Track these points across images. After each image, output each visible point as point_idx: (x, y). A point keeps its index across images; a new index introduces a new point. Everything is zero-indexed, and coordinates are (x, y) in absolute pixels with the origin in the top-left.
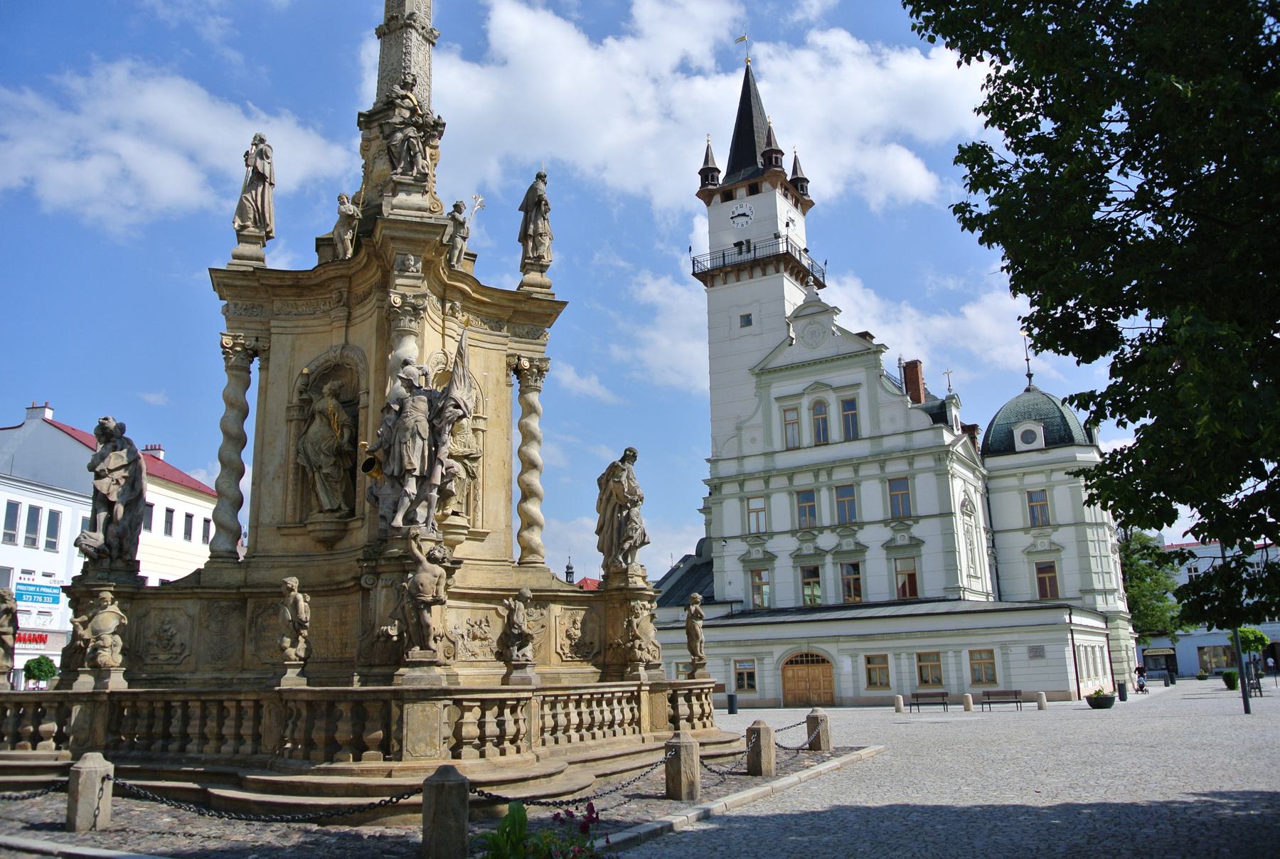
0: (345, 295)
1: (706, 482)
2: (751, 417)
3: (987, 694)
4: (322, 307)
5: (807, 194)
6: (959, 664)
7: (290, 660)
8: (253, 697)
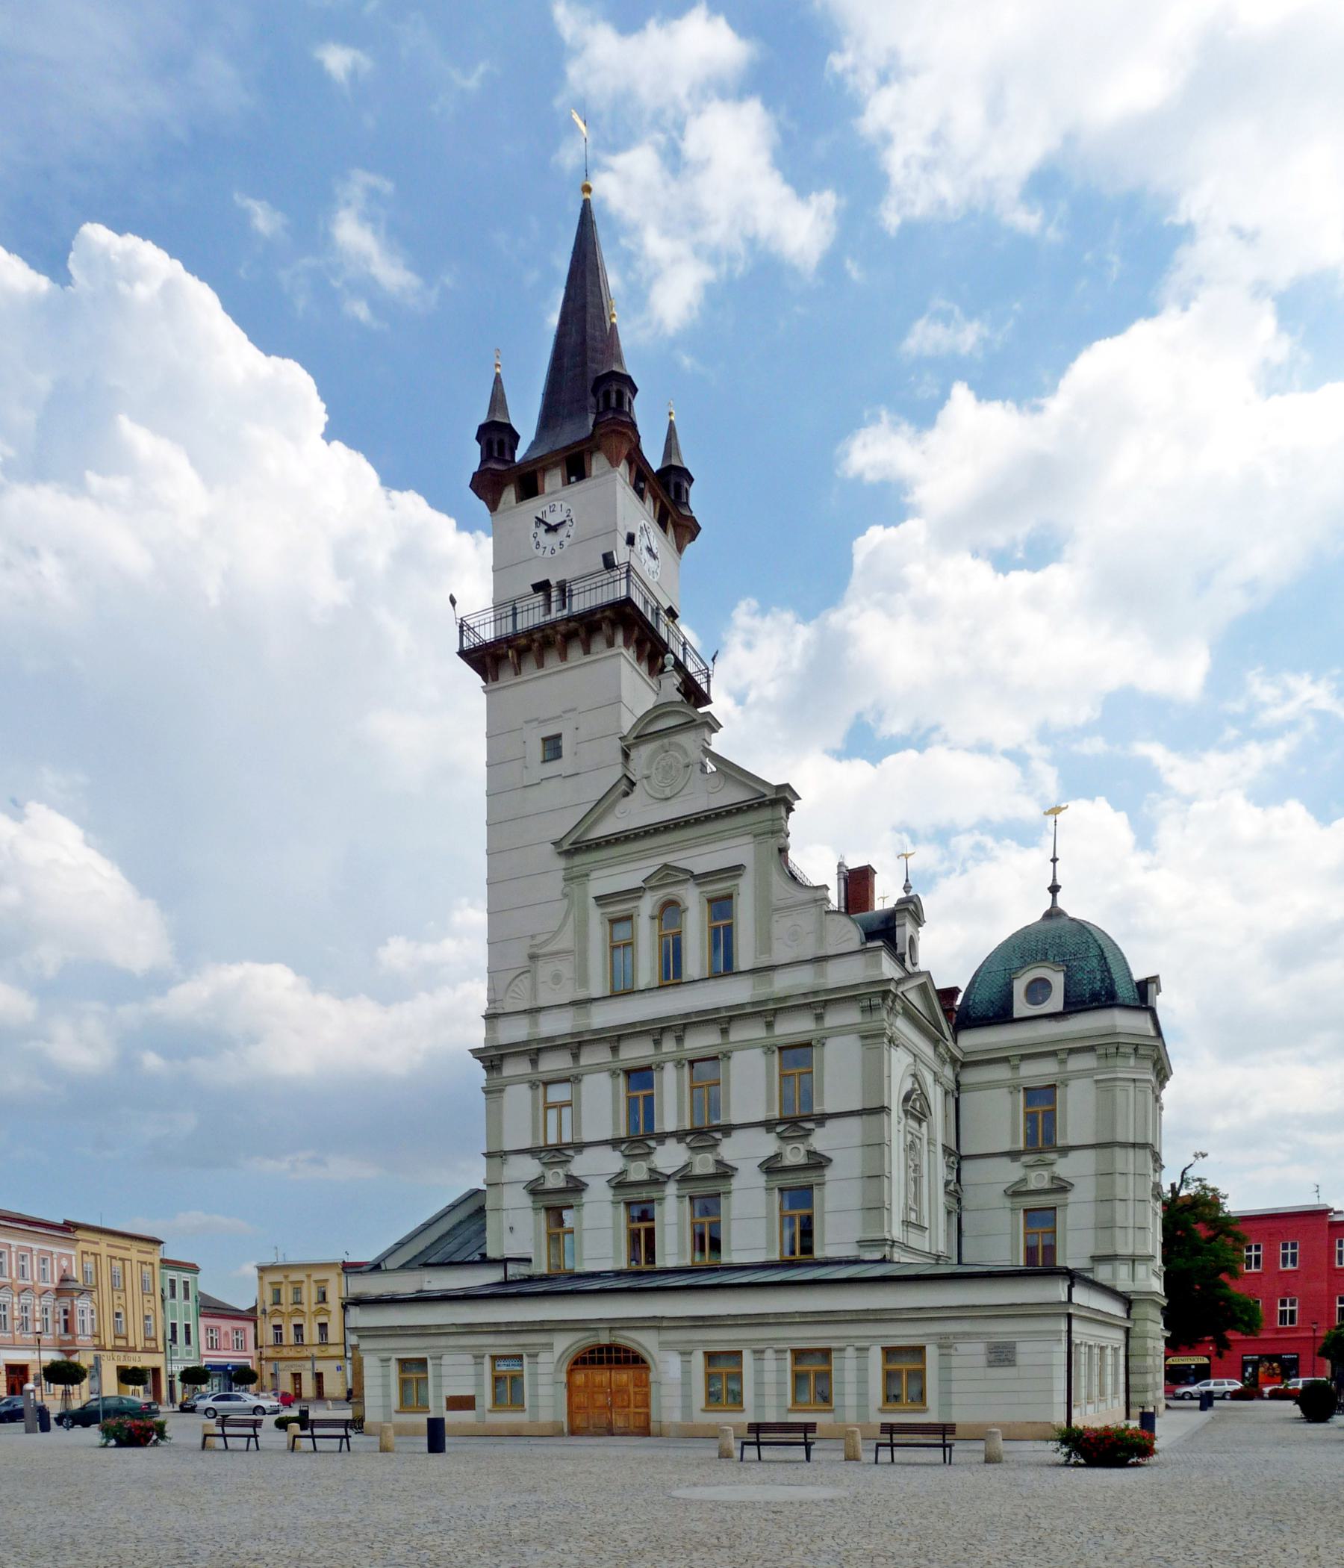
1: (477, 1053)
2: (556, 934)
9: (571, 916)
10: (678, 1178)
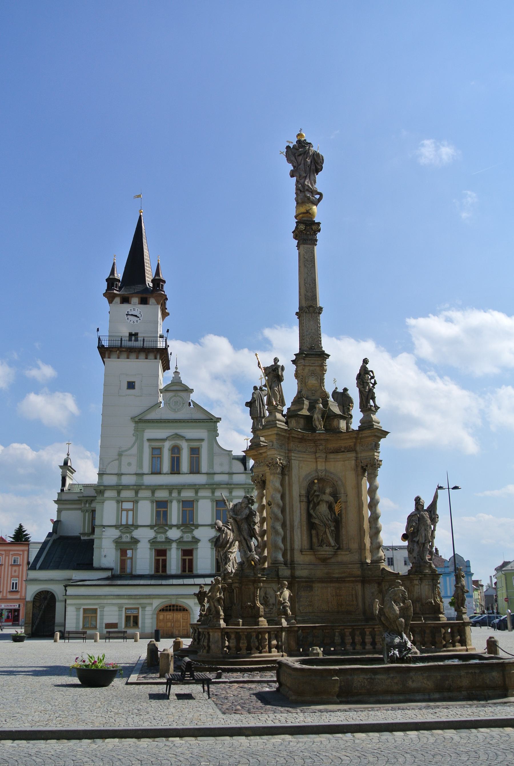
2: (130, 449)
9: (137, 443)
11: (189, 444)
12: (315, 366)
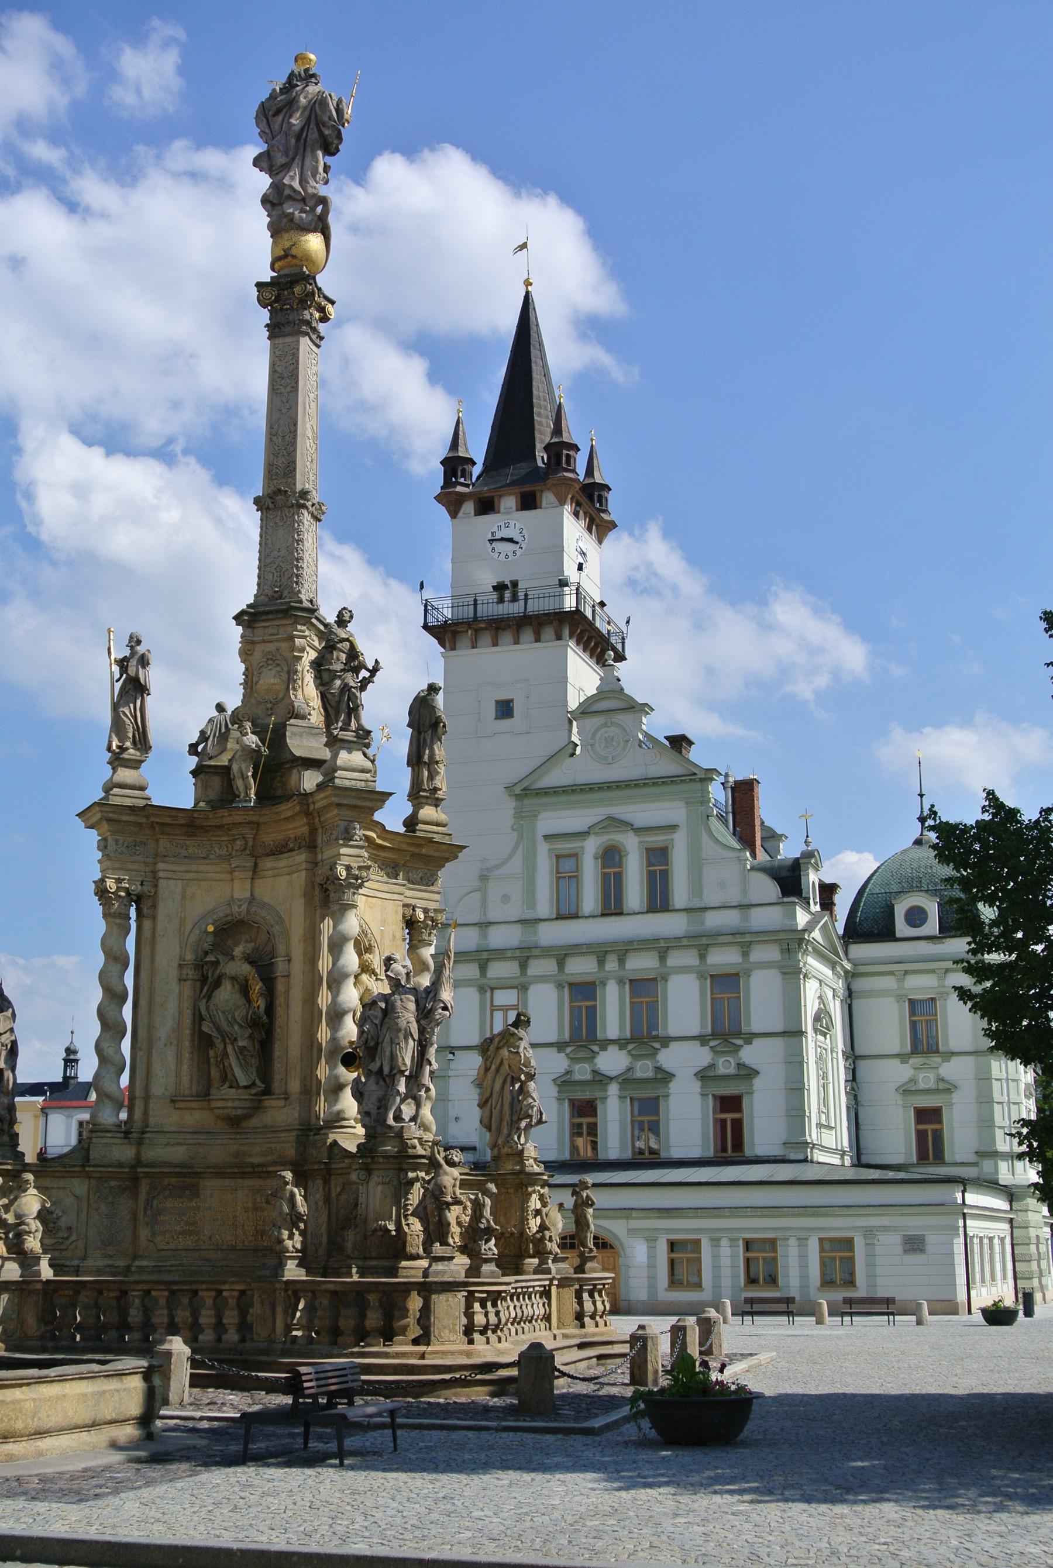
0: (250, 843)
2: (504, 862)
3: (849, 1301)
4: (217, 851)
5: (605, 511)
6: (803, 1257)
7: (288, 1252)
8: (238, 1287)
10: (620, 1081)
11: (641, 839)
12: (277, 641)
